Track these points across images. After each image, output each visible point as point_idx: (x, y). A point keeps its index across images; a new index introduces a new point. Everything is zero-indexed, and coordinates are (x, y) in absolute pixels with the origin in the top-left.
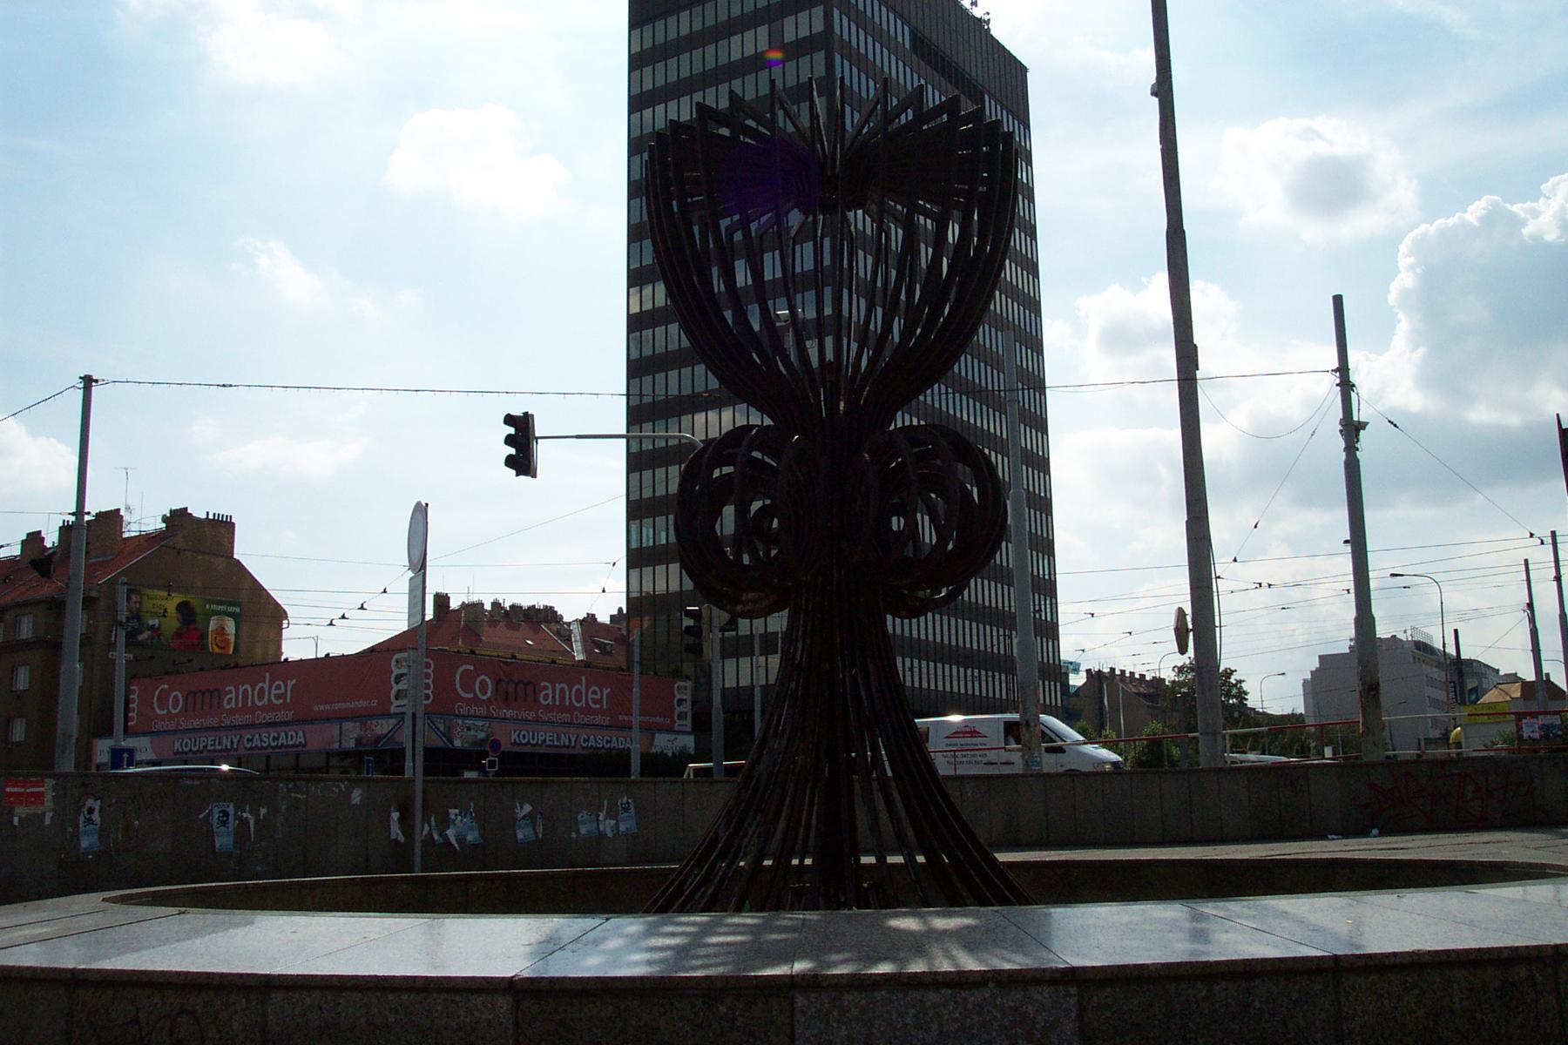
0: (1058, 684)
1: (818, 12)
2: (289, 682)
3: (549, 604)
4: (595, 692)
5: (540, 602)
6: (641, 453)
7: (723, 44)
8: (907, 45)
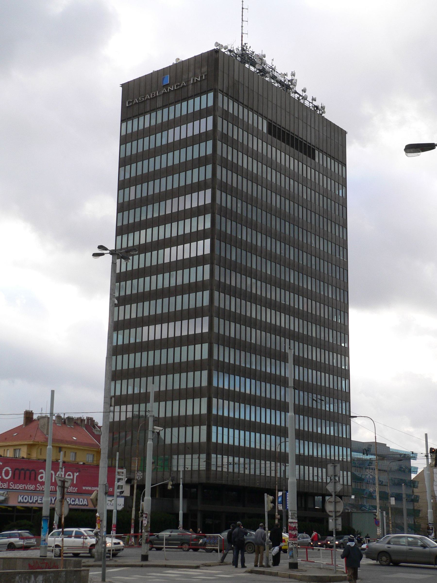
0: (349, 473)
1: (211, 95)
2: (75, 473)
4: (69, 475)
8: (265, 130)
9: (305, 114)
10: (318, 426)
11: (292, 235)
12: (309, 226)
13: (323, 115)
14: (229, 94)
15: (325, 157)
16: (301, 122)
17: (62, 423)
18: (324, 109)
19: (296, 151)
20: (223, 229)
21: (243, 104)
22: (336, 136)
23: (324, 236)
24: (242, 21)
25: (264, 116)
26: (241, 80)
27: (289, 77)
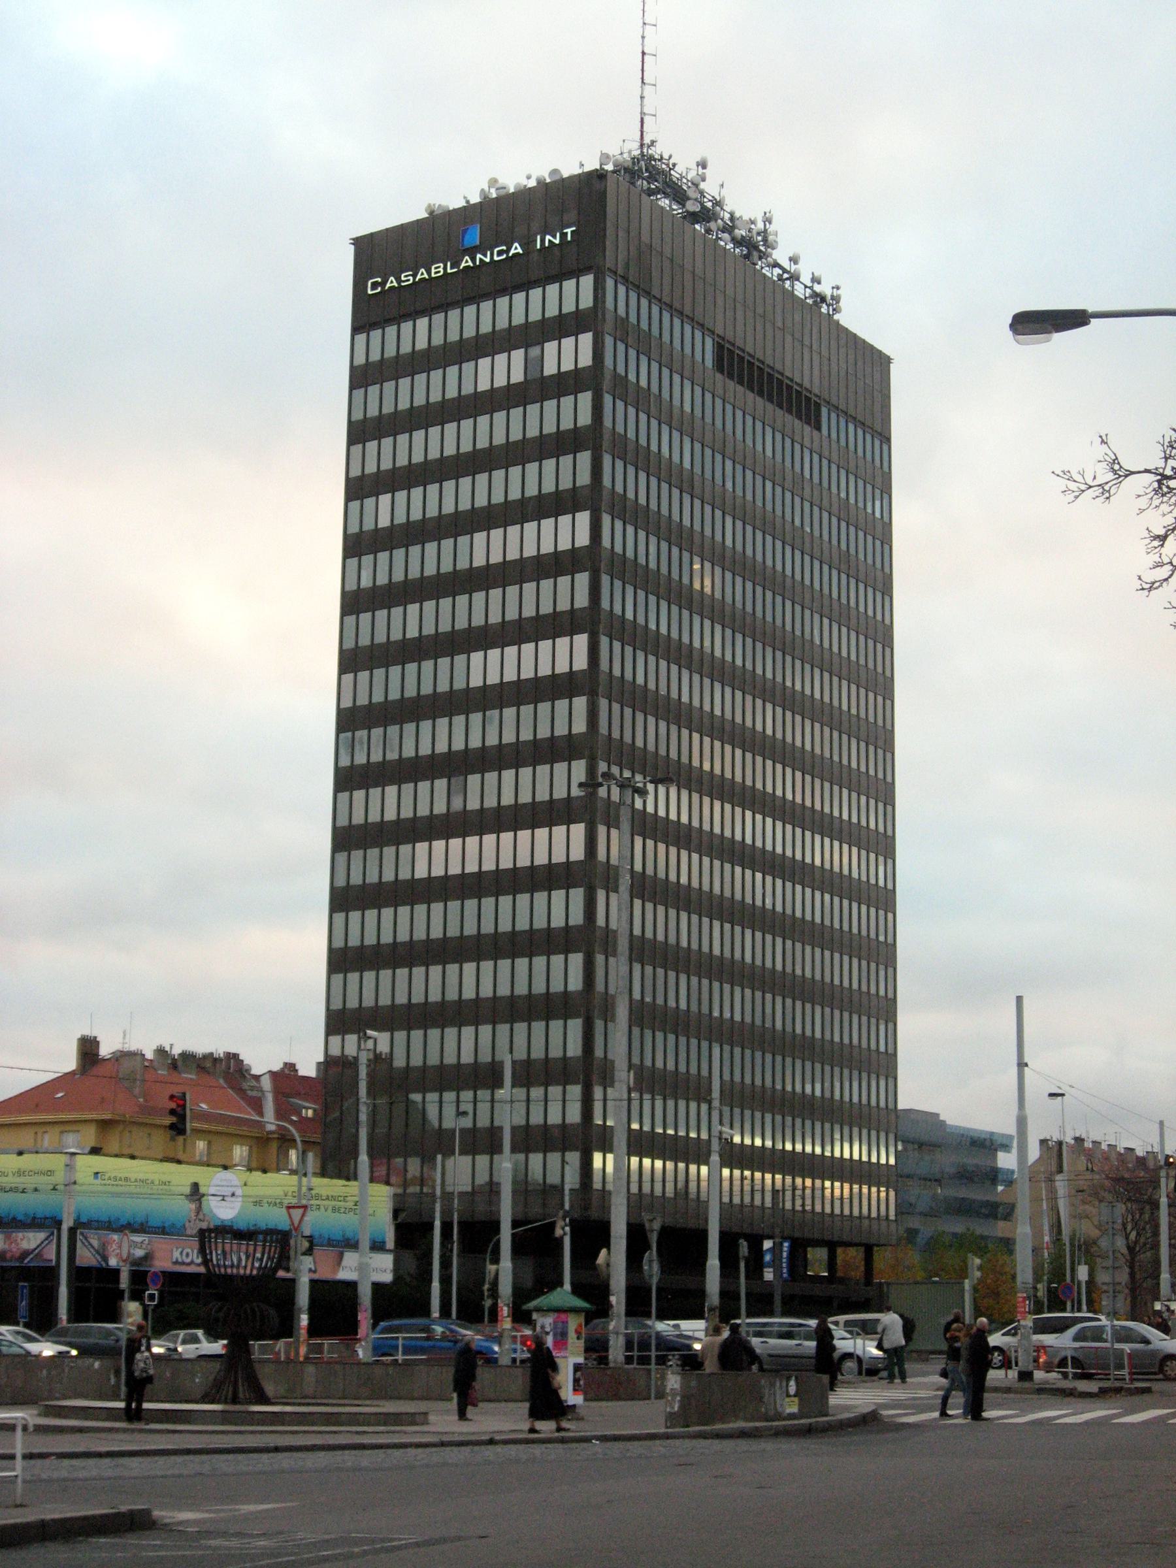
1: (587, 281)
3: (233, 1050)
5: (219, 1048)
6: (354, 709)
7: (468, 367)
8: (709, 362)
9: (797, 317)
10: (806, 1081)
11: (769, 618)
12: (808, 596)
13: (836, 317)
14: (631, 279)
15: (677, 322)
16: (789, 339)
17: (169, 1068)
18: (838, 302)
19: (759, 399)
20: (618, 609)
21: (660, 300)
22: (868, 370)
23: (841, 615)
24: (643, 82)
25: (643, 290)
26: (656, 243)
27: (760, 226)
